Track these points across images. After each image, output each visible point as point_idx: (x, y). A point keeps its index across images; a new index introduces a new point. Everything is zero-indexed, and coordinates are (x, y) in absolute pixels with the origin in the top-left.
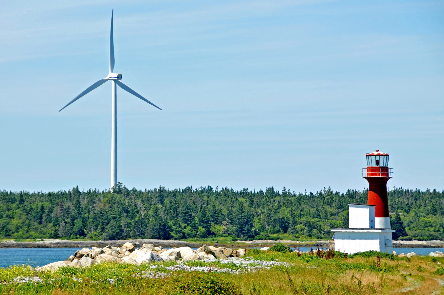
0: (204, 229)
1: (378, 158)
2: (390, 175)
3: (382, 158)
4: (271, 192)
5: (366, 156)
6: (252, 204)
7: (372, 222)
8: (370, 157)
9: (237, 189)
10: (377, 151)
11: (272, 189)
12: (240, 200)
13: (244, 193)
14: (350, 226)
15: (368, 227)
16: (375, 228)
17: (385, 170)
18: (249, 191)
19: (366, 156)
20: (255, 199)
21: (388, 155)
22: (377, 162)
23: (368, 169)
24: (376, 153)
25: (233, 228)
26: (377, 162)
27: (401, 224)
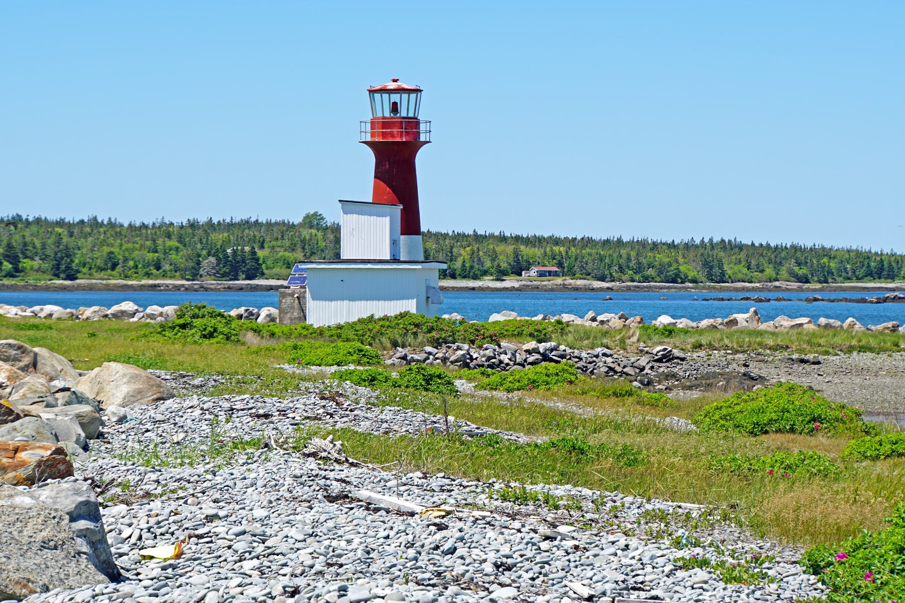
0: (10, 266)
1: (395, 98)
2: (423, 138)
3: (405, 96)
4: (95, 223)
5: (370, 91)
6: (71, 235)
7: (394, 243)
8: (377, 96)
9: (53, 217)
10: (395, 81)
11: (95, 218)
12: (56, 229)
13: (61, 223)
14: (344, 255)
15: (388, 258)
16: (402, 259)
17: (413, 124)
18: (67, 220)
19: (370, 91)
20: (76, 231)
21: (421, 91)
22: (395, 108)
23: (372, 123)
24: (392, 86)
25: (46, 265)
26: (395, 108)
27: (258, 259)
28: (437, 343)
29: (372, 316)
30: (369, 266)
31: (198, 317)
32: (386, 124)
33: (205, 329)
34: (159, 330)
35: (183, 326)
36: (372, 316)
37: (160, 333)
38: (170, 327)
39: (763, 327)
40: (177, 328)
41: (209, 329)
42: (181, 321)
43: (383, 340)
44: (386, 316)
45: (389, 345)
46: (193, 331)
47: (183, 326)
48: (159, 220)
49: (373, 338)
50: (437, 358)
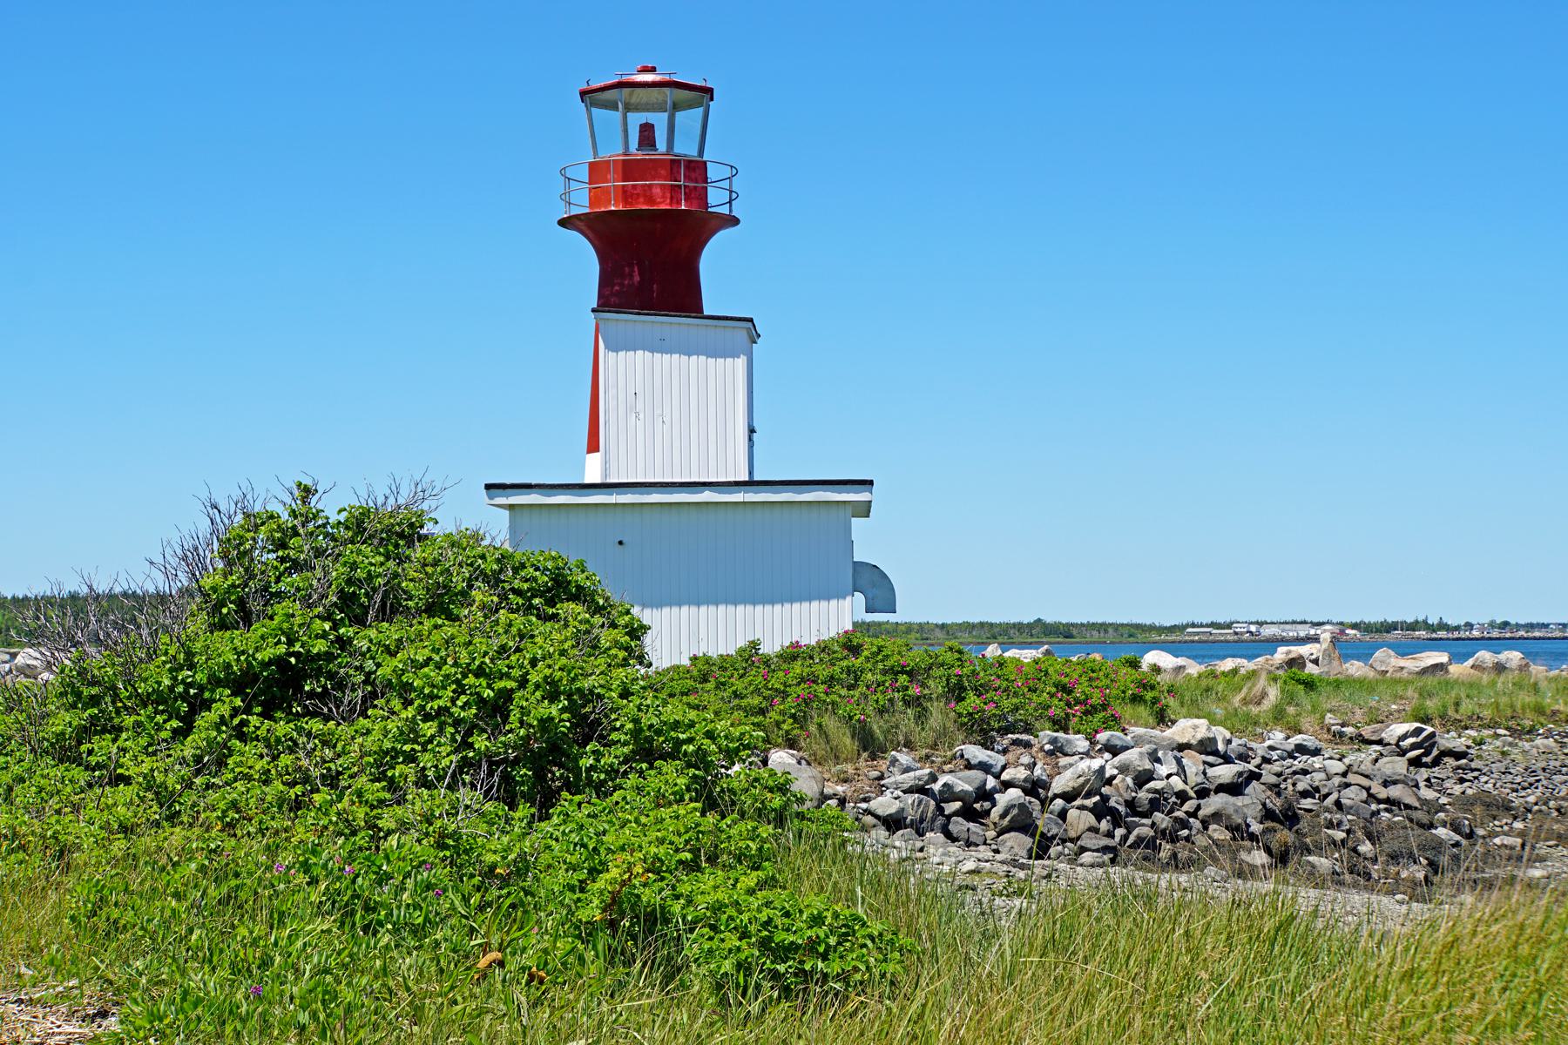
28: (983, 733)
29: (754, 645)
30: (707, 496)
31: (390, 609)
32: (629, 168)
33: (496, 710)
34: (64, 721)
35: (279, 687)
36: (754, 645)
37: (66, 751)
38: (158, 699)
39: (1355, 668)
40: (225, 703)
41: (534, 708)
42: (259, 644)
43: (830, 723)
44: (796, 645)
45: (848, 743)
46: (381, 728)
47: (279, 687)
48: (204, 526)
49: (800, 720)
50: (1007, 785)
